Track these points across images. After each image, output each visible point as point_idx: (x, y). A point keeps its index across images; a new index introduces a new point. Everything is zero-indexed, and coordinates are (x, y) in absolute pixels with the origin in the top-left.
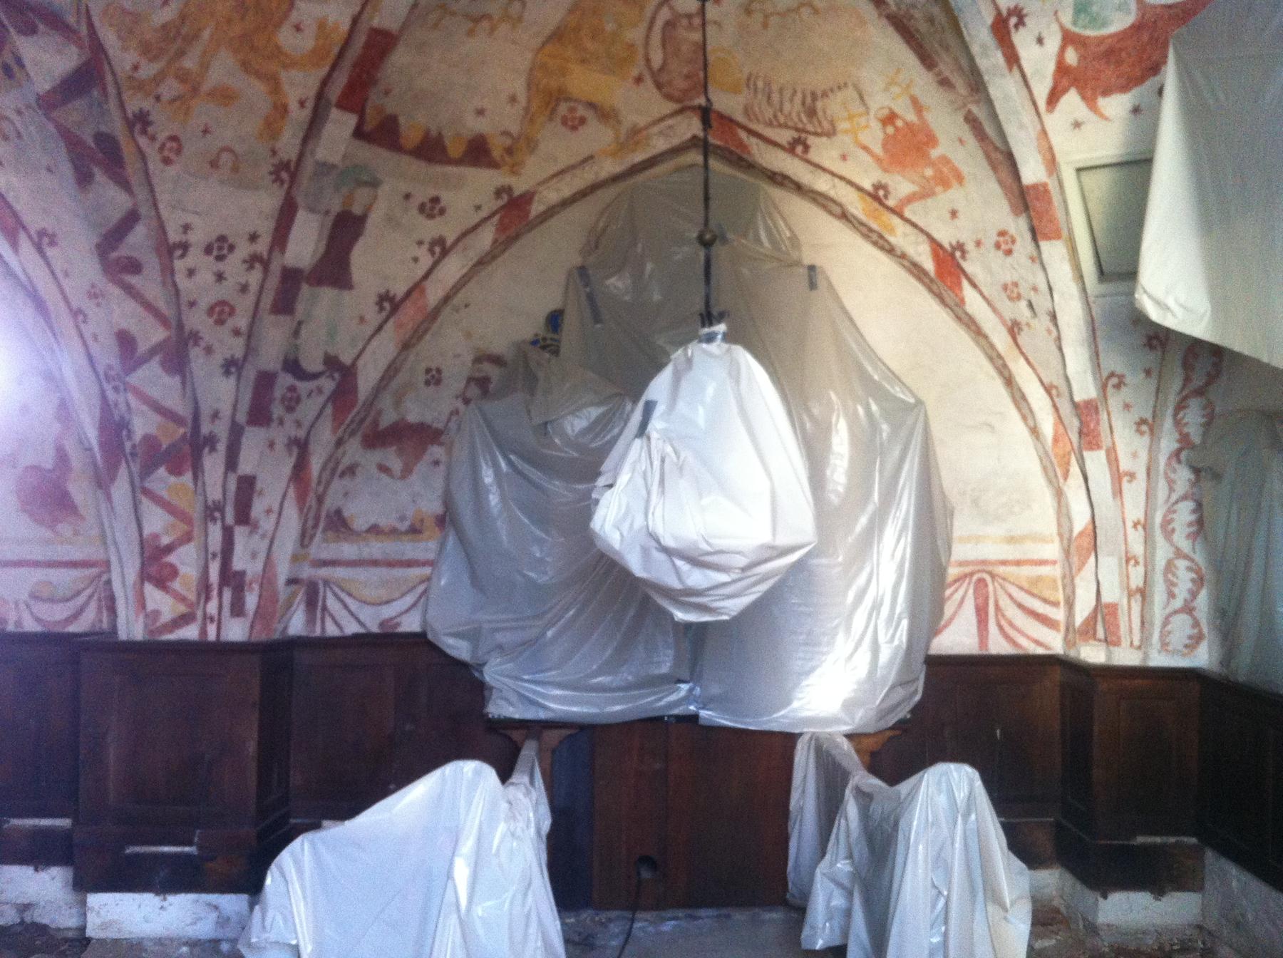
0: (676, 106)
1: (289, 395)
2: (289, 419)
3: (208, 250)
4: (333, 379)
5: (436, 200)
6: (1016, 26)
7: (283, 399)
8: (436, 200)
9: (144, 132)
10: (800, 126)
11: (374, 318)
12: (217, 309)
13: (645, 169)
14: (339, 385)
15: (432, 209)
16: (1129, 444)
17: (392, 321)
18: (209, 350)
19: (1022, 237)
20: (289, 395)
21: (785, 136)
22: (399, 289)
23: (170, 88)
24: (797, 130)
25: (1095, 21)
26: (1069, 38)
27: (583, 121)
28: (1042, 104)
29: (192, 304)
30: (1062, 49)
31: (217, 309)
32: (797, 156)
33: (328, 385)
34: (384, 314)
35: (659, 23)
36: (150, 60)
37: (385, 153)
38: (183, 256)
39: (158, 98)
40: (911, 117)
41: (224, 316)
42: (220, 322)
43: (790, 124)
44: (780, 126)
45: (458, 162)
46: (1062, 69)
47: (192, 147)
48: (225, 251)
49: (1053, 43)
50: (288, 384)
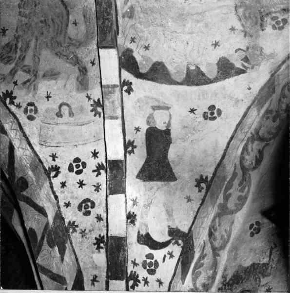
1: (148, 261)
3: (71, 169)
4: (179, 245)
9: (12, 103)
11: (197, 196)
12: (84, 205)
14: (183, 248)
15: (212, 114)
17: (209, 193)
20: (148, 261)
22: (209, 172)
23: (21, 76)
31: (84, 205)
33: (177, 250)
34: (204, 191)
36: (6, 64)
38: (56, 176)
39: (15, 83)
41: (90, 209)
42: (87, 213)
45: (216, 80)
47: (43, 106)
48: (81, 168)
50: (147, 253)
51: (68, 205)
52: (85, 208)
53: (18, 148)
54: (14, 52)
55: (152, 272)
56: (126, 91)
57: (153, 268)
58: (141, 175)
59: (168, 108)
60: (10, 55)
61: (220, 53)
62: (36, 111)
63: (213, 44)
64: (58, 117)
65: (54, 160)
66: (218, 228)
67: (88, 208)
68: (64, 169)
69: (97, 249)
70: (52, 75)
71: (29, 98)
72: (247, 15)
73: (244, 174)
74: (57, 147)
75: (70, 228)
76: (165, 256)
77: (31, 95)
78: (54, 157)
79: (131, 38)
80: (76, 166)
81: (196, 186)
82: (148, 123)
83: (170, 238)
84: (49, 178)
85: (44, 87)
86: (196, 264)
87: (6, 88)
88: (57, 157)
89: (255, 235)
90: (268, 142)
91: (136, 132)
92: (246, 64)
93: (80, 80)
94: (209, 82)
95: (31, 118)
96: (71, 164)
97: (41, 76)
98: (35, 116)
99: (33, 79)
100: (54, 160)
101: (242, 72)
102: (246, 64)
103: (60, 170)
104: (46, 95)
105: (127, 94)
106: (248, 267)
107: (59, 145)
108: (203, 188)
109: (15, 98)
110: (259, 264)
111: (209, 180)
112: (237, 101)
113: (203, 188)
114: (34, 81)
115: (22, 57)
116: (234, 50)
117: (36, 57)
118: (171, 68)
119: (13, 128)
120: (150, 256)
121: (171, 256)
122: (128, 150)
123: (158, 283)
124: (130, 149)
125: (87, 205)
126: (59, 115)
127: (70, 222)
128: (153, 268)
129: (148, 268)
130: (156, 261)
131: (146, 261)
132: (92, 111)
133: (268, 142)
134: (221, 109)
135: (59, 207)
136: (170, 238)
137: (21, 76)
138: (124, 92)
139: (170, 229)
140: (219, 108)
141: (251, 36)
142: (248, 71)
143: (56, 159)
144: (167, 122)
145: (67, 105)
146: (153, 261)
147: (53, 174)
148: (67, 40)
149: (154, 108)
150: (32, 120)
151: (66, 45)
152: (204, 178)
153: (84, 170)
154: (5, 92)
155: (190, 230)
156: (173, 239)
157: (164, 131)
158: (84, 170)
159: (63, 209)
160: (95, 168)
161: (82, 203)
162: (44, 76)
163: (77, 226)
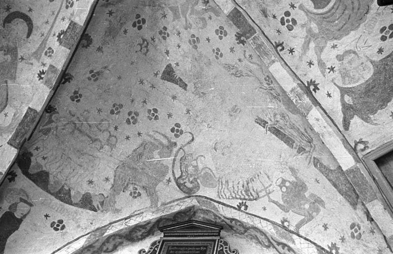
0: (187, 195)
5: (61, 222)
6: (314, 90)
8: (61, 222)
10: (242, 197)
15: (58, 225)
19: (362, 222)
21: (235, 203)
24: (241, 199)
25: (352, 79)
26: (344, 91)
27: (139, 195)
28: (342, 129)
30: (342, 97)
32: (242, 211)
35: (179, 157)
40: (293, 179)
43: (238, 197)
44: (233, 198)
45: (76, 205)
46: (346, 108)
49: (337, 95)
56: (9, 179)
59: (31, 205)
82: (10, 208)
92: (100, 206)
94: (71, 204)
101: (96, 211)
102: (100, 206)
105: (8, 181)
118: (51, 178)
140: (65, 224)
142: (99, 212)
149: (22, 200)
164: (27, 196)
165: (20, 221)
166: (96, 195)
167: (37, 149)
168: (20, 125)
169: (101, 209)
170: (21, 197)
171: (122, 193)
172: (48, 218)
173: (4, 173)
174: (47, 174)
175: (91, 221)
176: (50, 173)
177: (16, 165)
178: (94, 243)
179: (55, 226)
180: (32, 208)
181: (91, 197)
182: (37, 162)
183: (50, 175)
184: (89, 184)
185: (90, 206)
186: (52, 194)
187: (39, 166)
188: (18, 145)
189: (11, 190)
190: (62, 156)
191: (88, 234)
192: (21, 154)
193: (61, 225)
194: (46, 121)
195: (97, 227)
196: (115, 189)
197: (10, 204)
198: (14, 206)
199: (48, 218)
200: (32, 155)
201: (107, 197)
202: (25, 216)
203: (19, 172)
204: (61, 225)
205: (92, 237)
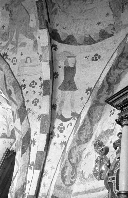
1: (61, 127)
2: (61, 134)
3: (30, 86)
4: (75, 120)
5: (96, 55)
7: (58, 128)
9: (7, 58)
13: (13, 76)
15: (96, 58)
16: (58, 94)
18: (33, 113)
20: (61, 127)
23: (11, 46)
29: (28, 101)
34: (89, 95)
37: (74, 47)
38: (24, 89)
39: (8, 49)
41: (37, 103)
42: (36, 105)
48: (35, 85)
51: (28, 101)
52: (35, 103)
53: (7, 77)
54: (8, 36)
55: (61, 132)
56: (54, 49)
57: (62, 130)
58: (60, 88)
59: (75, 57)
60: (6, 37)
61: (101, 27)
62: (17, 61)
63: (97, 24)
64: (26, 63)
65: (24, 82)
66: (94, 112)
67: (36, 102)
68: (28, 86)
69: (38, 120)
70: (24, 44)
71: (14, 56)
72: (115, 6)
73: (109, 86)
74: (25, 76)
75: (28, 111)
76: (68, 125)
77: (14, 54)
78: (23, 80)
79: (57, 24)
80: (33, 84)
81: (86, 93)
82: (65, 64)
83: (72, 116)
84: (21, 89)
85: (20, 50)
86: (80, 128)
87: (4, 52)
88: (25, 81)
89: (112, 116)
90: (124, 70)
91: (59, 68)
92: (113, 31)
93: (34, 46)
94: (95, 42)
95: (14, 64)
96: (30, 84)
97: (19, 46)
98: (16, 63)
99: (16, 47)
100: (24, 82)
101: (112, 35)
102: (113, 31)
103: (26, 86)
104: (21, 54)
105: (55, 50)
106: (105, 131)
107: (25, 75)
108: (89, 93)
109: (8, 56)
110: (110, 129)
111: (92, 89)
112: (108, 50)
113: (89, 93)
114: (16, 48)
115: (11, 38)
116: (108, 25)
117: (17, 38)
118: (76, 37)
119: (6, 68)
120: (61, 125)
121: (71, 124)
122: (55, 76)
123: (64, 137)
124: (56, 76)
125: (36, 101)
126: (26, 62)
127: (28, 109)
128: (62, 130)
129: (60, 130)
130: (64, 127)
131: (59, 127)
132: (39, 59)
133: (124, 70)
134: (100, 55)
135: (24, 102)
136: (72, 116)
137: (11, 46)
138: (53, 50)
139: (72, 112)
140: (99, 55)
141: (117, 16)
142: (115, 34)
143: (24, 81)
144: (74, 63)
145: (29, 58)
146: (63, 127)
147: (23, 88)
148: (29, 29)
149: (68, 57)
150: (15, 65)
151: (29, 30)
152: (90, 89)
153: (36, 86)
154: (4, 53)
155: (81, 113)
156: (73, 117)
157: (72, 68)
158: (36, 86)
159: (26, 103)
160: (41, 85)
161: (34, 100)
162: (20, 46)
163: (31, 110)
164: (70, 53)
165: (74, 68)
166: (107, 27)
167: (57, 25)
168: (38, 15)
169: (115, 32)
170: (67, 55)
171: (122, 14)
172: (88, 58)
173: (48, 45)
174: (72, 36)
175: (114, 43)
176: (73, 34)
177: (52, 40)
178: (124, 50)
179: (95, 59)
180: (76, 58)
181: (105, 31)
182: (62, 33)
183: (74, 36)
184: (98, 25)
185: (107, 36)
186: (82, 45)
187: (65, 34)
188: (45, 26)
189: (59, 55)
190: (73, 21)
191: (116, 50)
192: (51, 33)
193: (98, 57)
194: (51, 6)
195: (119, 43)
196: (117, 15)
197: (64, 62)
198: (66, 62)
199: (88, 58)
200: (57, 30)
201: (115, 23)
202: (75, 64)
203: (56, 43)
204: (98, 57)
205: (119, 49)
